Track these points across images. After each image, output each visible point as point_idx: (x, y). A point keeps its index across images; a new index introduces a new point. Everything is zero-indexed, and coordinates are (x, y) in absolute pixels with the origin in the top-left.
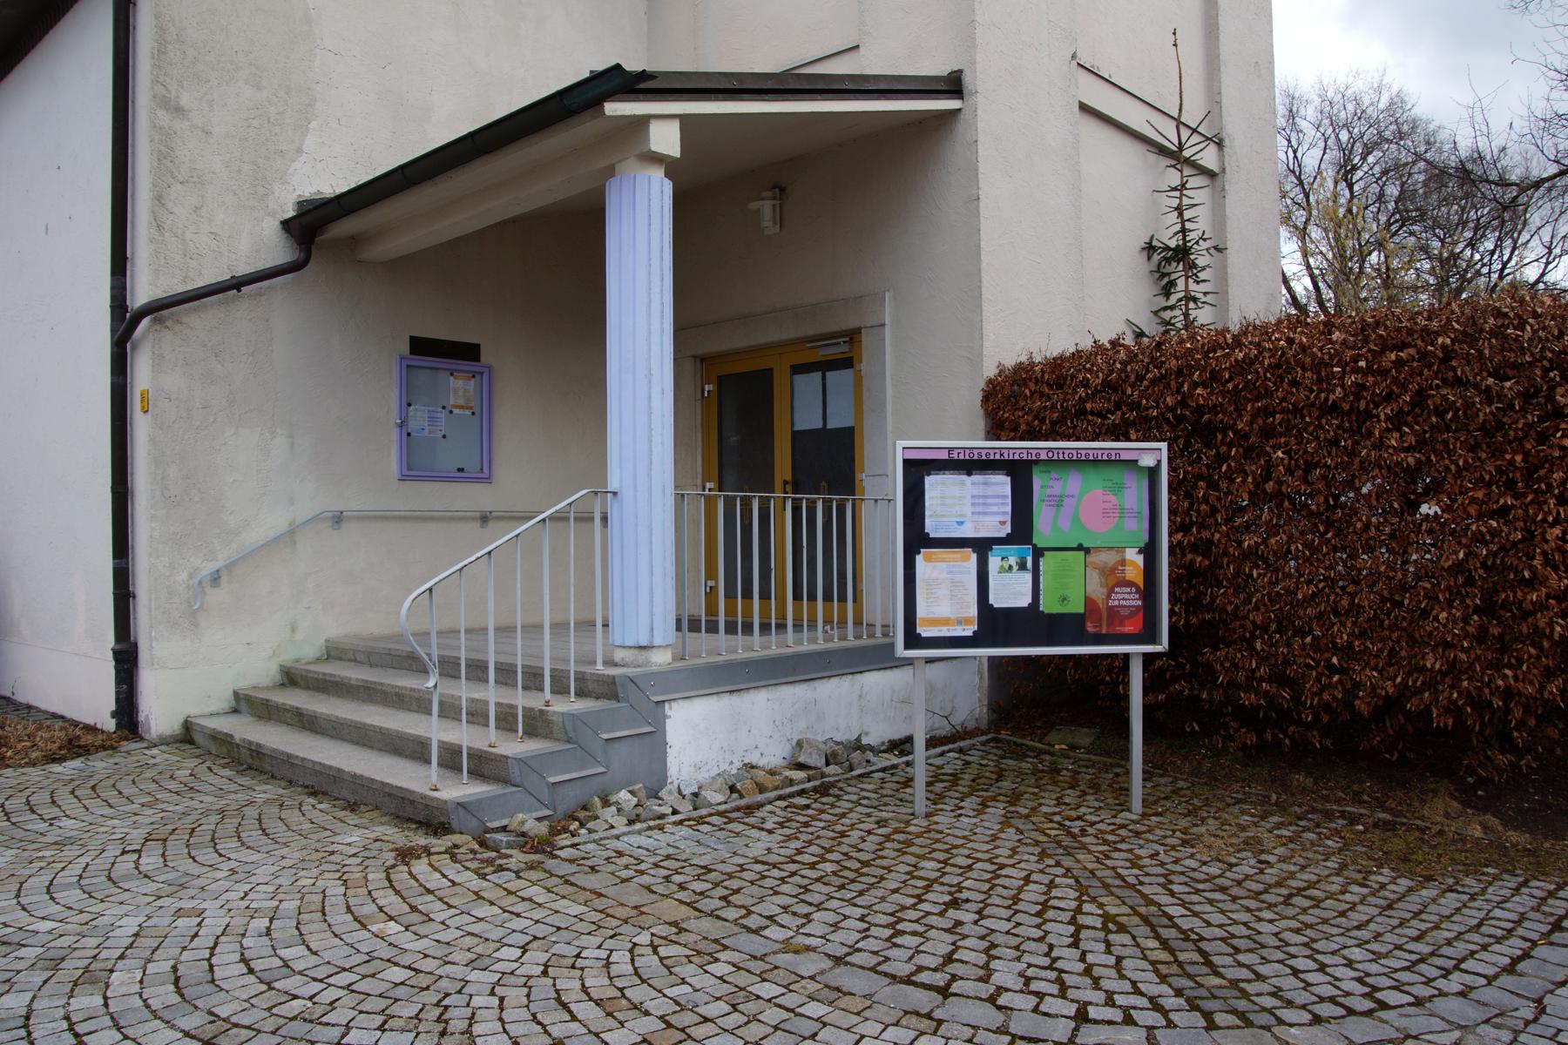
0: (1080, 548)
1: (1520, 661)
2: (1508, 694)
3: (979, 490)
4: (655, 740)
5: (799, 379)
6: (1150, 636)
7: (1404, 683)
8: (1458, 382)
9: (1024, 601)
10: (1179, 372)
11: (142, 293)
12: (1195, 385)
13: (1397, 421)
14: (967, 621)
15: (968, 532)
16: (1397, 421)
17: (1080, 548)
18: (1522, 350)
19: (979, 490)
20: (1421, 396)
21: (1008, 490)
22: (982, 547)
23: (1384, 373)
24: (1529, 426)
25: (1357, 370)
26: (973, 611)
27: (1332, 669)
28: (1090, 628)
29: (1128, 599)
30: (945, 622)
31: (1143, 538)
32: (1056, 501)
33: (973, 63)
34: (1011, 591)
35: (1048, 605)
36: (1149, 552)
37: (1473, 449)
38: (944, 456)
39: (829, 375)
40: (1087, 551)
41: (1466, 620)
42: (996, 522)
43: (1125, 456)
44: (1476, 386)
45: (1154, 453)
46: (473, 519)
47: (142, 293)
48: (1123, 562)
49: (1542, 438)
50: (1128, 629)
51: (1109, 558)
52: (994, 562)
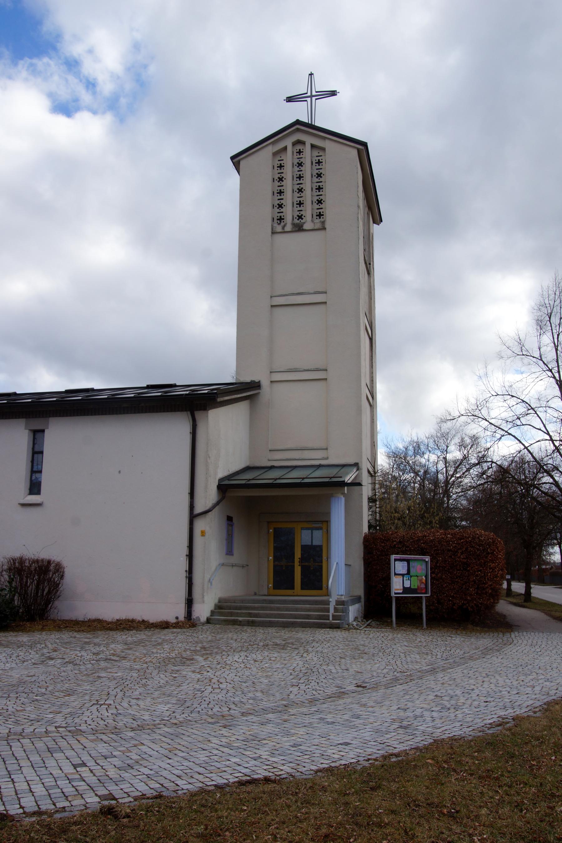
0: (416, 576)
1: (483, 598)
2: (481, 604)
3: (403, 565)
4: (519, 580)
5: (303, 531)
6: (426, 593)
7: (464, 603)
8: (472, 547)
9: (409, 586)
10: (417, 541)
11: (198, 509)
12: (421, 543)
13: (462, 553)
14: (401, 590)
15: (401, 573)
16: (462, 553)
17: (416, 576)
18: (482, 542)
19: (403, 565)
20: (467, 549)
21: (406, 565)
22: (403, 575)
23: (459, 544)
24: (484, 555)
25: (455, 543)
26: (402, 588)
27: (450, 600)
28: (418, 591)
29: (423, 586)
30: (398, 590)
31: (425, 574)
32: (413, 567)
33: (362, 462)
34: (407, 584)
35: (412, 587)
36: (426, 577)
37: (475, 559)
38: (399, 558)
39: (314, 531)
40: (417, 576)
41: (474, 590)
42: (405, 571)
43: (424, 559)
44: (476, 548)
45: (427, 558)
46: (230, 566)
47: (198, 509)
48: (422, 579)
49: (486, 557)
50: (423, 592)
51: (420, 578)
52: (405, 578)
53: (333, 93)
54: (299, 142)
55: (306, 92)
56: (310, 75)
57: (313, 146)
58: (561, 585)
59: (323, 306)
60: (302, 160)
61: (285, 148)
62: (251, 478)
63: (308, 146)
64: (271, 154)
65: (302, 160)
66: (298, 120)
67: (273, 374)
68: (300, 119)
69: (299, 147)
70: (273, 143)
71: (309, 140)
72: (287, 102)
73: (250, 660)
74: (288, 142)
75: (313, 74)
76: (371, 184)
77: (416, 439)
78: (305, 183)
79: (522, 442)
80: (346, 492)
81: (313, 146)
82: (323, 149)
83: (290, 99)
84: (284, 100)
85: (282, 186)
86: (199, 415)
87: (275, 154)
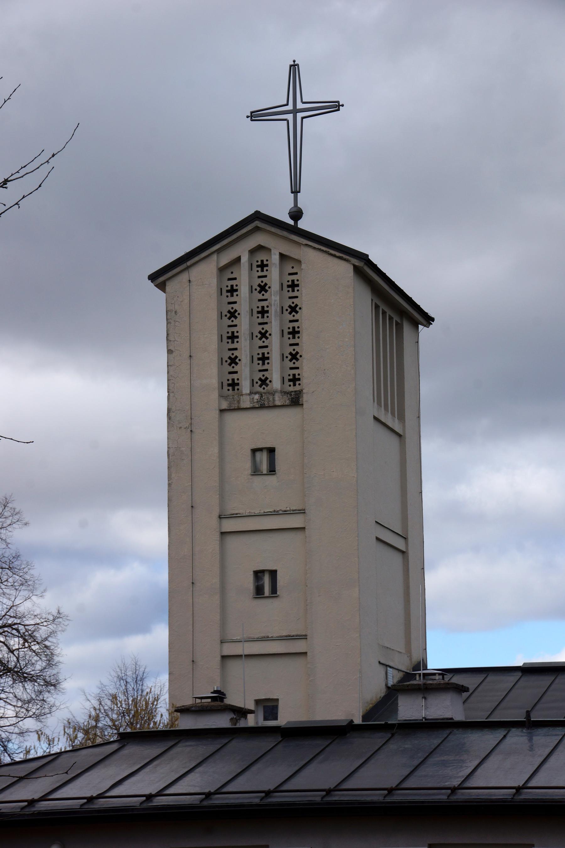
53: (336, 106)
54: (260, 248)
56: (291, 66)
59: (298, 536)
60: (236, 353)
61: (238, 259)
62: (36, 797)
63: (275, 258)
64: (215, 271)
65: (236, 353)
67: (226, 645)
68: (263, 211)
69: (261, 256)
70: (219, 251)
73: (146, 686)
75: (298, 65)
78: (271, 322)
79: (17, 604)
81: (282, 256)
82: (299, 262)
83: (254, 116)
85: (236, 326)
86: (186, 266)
87: (222, 270)
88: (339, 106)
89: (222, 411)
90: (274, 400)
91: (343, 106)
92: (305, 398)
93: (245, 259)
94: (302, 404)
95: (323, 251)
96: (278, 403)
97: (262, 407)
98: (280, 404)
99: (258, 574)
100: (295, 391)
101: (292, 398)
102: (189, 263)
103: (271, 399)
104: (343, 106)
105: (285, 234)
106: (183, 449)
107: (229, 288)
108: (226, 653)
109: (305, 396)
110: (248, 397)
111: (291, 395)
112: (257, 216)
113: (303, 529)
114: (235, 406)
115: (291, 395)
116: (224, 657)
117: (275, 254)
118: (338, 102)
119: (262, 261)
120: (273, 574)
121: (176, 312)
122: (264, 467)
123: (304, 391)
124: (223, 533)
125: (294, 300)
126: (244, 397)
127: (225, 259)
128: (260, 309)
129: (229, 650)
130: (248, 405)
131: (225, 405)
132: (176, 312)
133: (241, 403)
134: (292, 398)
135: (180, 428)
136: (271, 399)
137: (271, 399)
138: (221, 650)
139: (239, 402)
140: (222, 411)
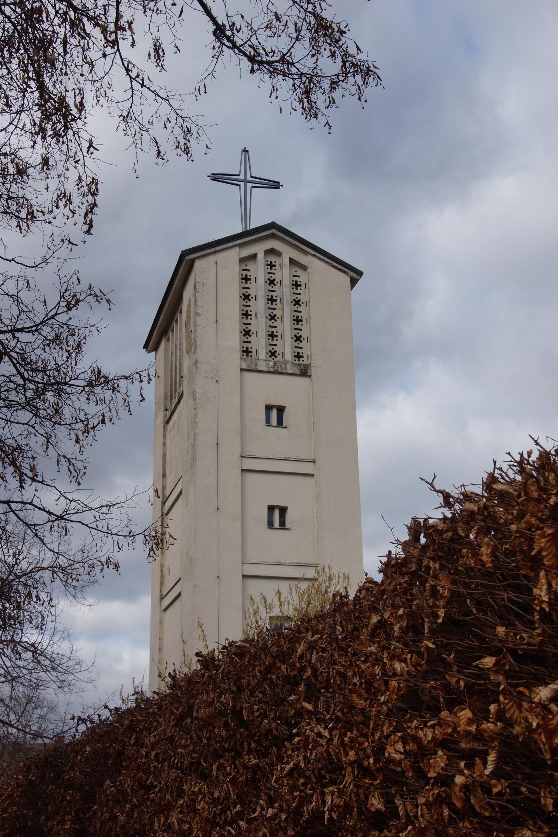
54: (271, 252)
55: (238, 173)
56: (244, 151)
57: (292, 262)
58: (553, 680)
61: (254, 257)
63: (286, 261)
66: (273, 223)
67: (246, 566)
70: (241, 246)
71: (288, 252)
72: (212, 179)
74: (259, 249)
76: (169, 299)
77: (226, 643)
80: (500, 689)
81: (292, 262)
82: (304, 268)
84: (208, 176)
87: (242, 260)
88: (279, 185)
89: (242, 370)
90: (286, 368)
91: (282, 186)
92: (313, 371)
93: (261, 256)
94: (310, 376)
95: (327, 262)
96: (289, 371)
97: (276, 372)
98: (291, 372)
99: (271, 509)
100: (304, 364)
101: (301, 369)
102: (217, 248)
103: (283, 366)
104: (282, 186)
105: (297, 243)
106: (209, 395)
107: (249, 277)
108: (246, 573)
109: (312, 368)
110: (264, 362)
111: (300, 367)
112: (273, 225)
113: (313, 475)
114: (253, 368)
115: (300, 367)
116: (244, 576)
117: (286, 257)
118: (278, 183)
119: (271, 262)
120: (283, 510)
121: (203, 284)
122: (277, 524)
123: (312, 365)
124: (243, 470)
125: (297, 296)
126: (261, 362)
127: (247, 252)
128: (274, 298)
129: (250, 570)
130: (264, 368)
131: (244, 366)
132: (203, 284)
133: (258, 366)
134: (301, 369)
135: (207, 377)
136: (284, 367)
137: (284, 367)
138: (242, 570)
139: (256, 365)
140: (242, 370)
